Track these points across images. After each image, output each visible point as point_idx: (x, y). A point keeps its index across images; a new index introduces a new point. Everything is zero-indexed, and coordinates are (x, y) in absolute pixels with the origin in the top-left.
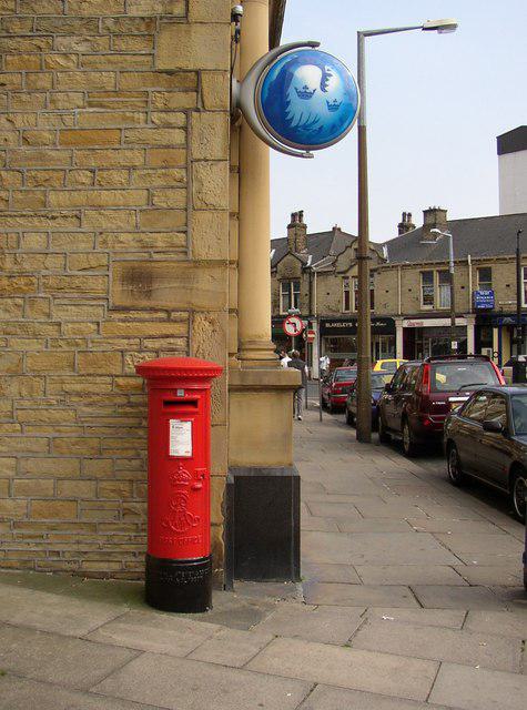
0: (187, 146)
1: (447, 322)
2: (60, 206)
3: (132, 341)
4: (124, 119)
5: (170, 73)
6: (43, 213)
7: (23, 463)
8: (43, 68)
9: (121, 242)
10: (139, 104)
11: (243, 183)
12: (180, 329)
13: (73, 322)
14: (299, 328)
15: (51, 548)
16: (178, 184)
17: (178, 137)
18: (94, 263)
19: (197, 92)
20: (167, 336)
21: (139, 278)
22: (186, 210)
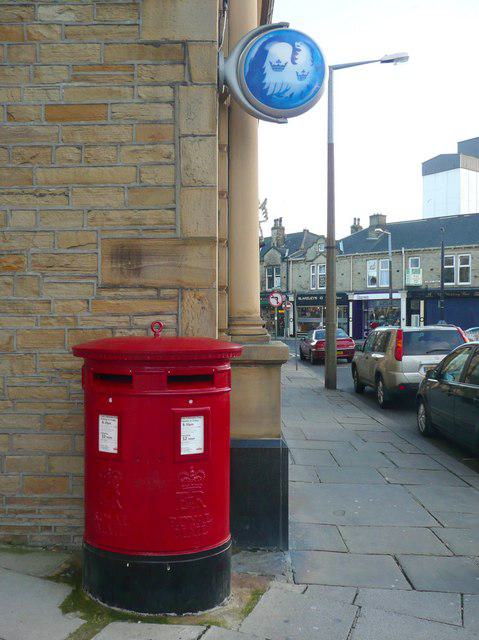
0: (174, 121)
1: (386, 296)
2: (47, 183)
3: (122, 319)
4: (111, 93)
5: (156, 44)
6: (30, 191)
7: (15, 439)
8: (28, 39)
9: (110, 220)
10: (124, 77)
11: (233, 163)
12: (171, 306)
13: (63, 300)
14: (280, 300)
15: (44, 523)
16: (167, 161)
17: (166, 112)
18: (82, 242)
19: (184, 64)
20: (157, 314)
21: (128, 256)
22: (174, 186)
